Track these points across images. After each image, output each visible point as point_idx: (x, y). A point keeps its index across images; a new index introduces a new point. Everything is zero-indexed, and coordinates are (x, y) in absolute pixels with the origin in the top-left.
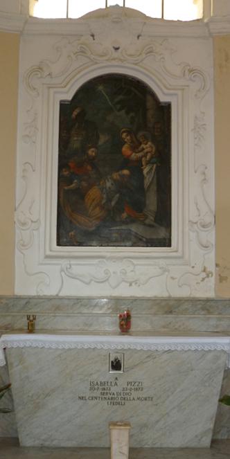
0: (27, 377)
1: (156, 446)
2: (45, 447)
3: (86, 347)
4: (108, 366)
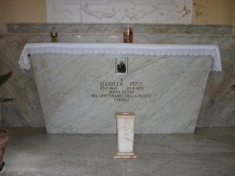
0: (49, 79)
1: (152, 133)
2: (66, 134)
3: (96, 53)
4: (115, 69)
